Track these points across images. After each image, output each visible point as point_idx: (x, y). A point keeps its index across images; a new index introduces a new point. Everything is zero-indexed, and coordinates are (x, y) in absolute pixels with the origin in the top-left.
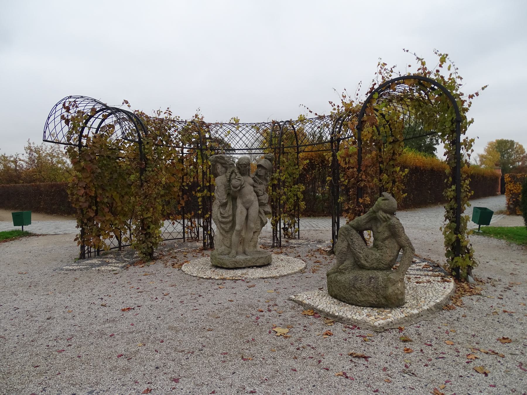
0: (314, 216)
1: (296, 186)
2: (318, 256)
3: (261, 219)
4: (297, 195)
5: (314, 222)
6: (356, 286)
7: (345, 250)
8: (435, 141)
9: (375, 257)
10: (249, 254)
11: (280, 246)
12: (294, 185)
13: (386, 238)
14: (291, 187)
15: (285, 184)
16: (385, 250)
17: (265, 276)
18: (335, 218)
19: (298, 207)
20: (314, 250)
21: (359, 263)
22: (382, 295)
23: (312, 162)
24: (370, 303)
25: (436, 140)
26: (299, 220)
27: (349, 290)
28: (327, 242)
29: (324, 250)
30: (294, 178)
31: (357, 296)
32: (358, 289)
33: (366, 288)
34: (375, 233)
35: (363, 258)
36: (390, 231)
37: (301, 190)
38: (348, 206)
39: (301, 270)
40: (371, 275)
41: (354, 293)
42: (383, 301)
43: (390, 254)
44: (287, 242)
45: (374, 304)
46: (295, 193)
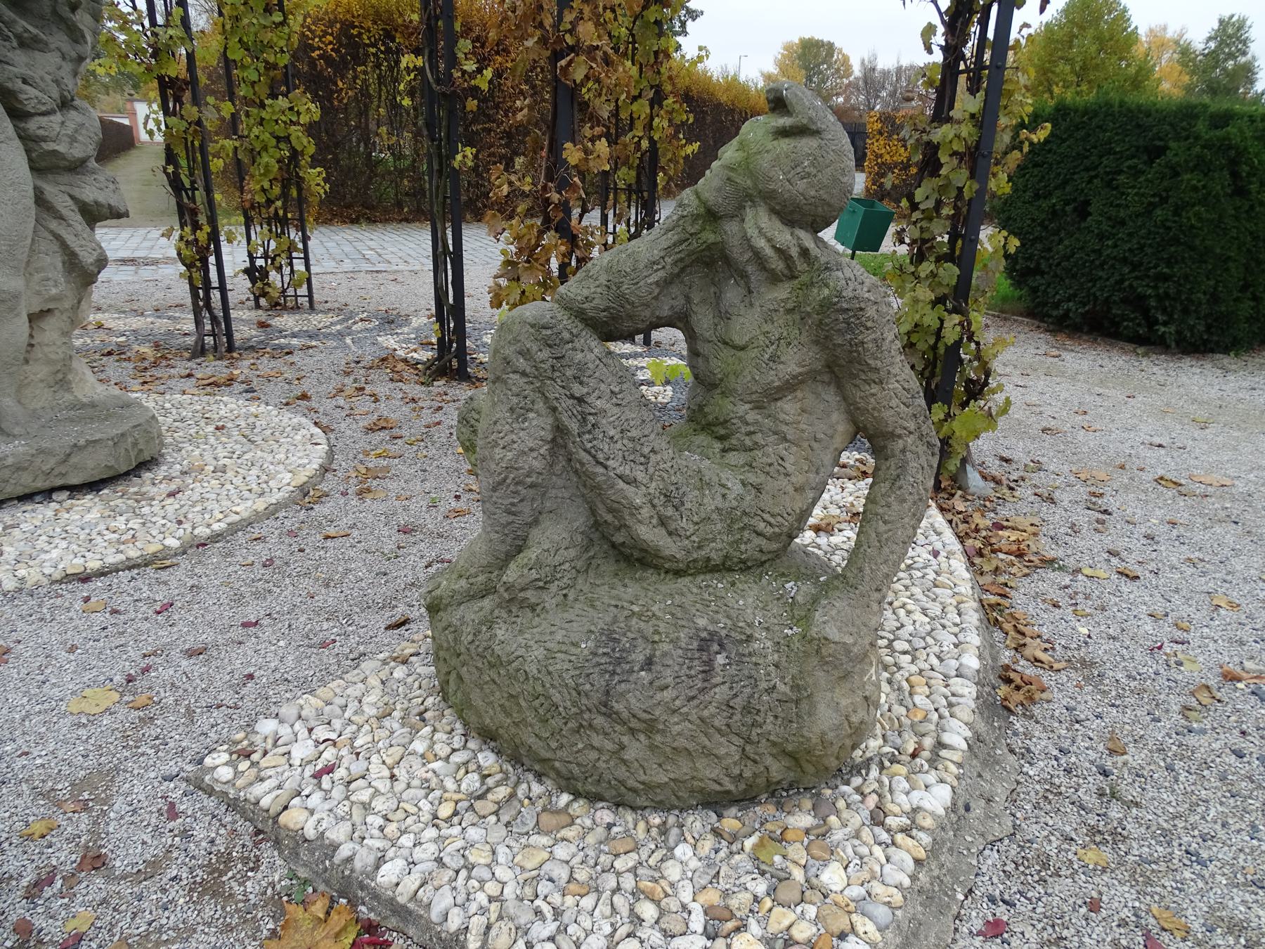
0: (372, 221)
1: (282, 102)
2: (382, 389)
3: (64, 245)
4: (287, 139)
5: (371, 243)
6: (616, 706)
7: (538, 465)
8: (678, 24)
9: (719, 502)
10: (17, 430)
11: (231, 348)
12: (274, 96)
13: (790, 387)
14: (262, 106)
15: (236, 90)
16: (773, 449)
17: (94, 564)
18: (444, 233)
19: (300, 190)
20: (368, 359)
21: (619, 538)
22: (774, 744)
23: (352, 36)
24: (702, 791)
25: (681, 21)
26: (305, 239)
27: (572, 724)
28: (415, 322)
29: (405, 361)
30: (270, 66)
31: (624, 762)
32: (634, 724)
33: (686, 718)
34: (703, 348)
35: (646, 512)
36: (822, 341)
37: (304, 119)
38: (510, 183)
39: (303, 490)
40: (702, 622)
41: (609, 746)
42: (777, 769)
43: (798, 479)
44: (263, 325)
45: (728, 792)
46: (280, 130)
